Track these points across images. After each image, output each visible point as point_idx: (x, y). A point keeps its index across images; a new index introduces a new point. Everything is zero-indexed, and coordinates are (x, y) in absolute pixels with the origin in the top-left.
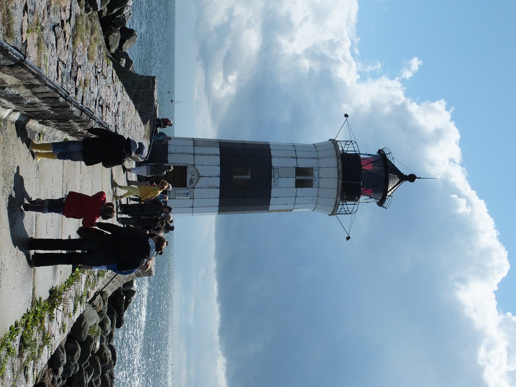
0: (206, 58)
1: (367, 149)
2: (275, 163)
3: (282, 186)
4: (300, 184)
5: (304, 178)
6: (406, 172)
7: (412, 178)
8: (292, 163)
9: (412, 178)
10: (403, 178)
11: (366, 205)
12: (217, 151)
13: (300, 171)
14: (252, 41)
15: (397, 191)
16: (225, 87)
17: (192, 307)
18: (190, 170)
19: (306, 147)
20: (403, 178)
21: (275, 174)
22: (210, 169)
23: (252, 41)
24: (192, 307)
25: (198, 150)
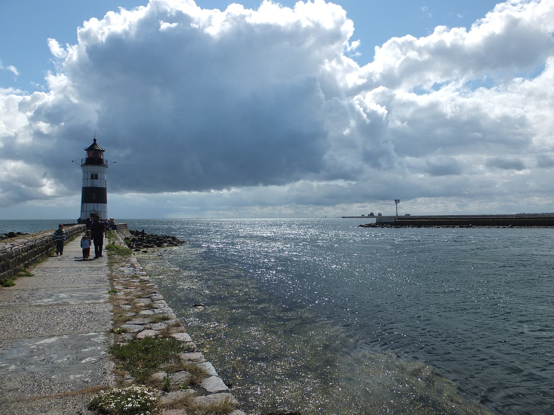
0: (23, 197)
1: (84, 155)
2: (89, 186)
3: (97, 184)
4: (97, 178)
5: (95, 177)
6: (93, 142)
7: (95, 140)
8: (89, 180)
9: (95, 140)
10: (95, 144)
11: (105, 156)
12: (85, 204)
13: (92, 178)
14: (13, 167)
15: (100, 146)
16: (48, 187)
17: (187, 207)
18: (92, 213)
19: (84, 175)
20: (95, 144)
21: (93, 186)
22: (91, 207)
23: (13, 167)
24: (187, 207)
25: (85, 210)
